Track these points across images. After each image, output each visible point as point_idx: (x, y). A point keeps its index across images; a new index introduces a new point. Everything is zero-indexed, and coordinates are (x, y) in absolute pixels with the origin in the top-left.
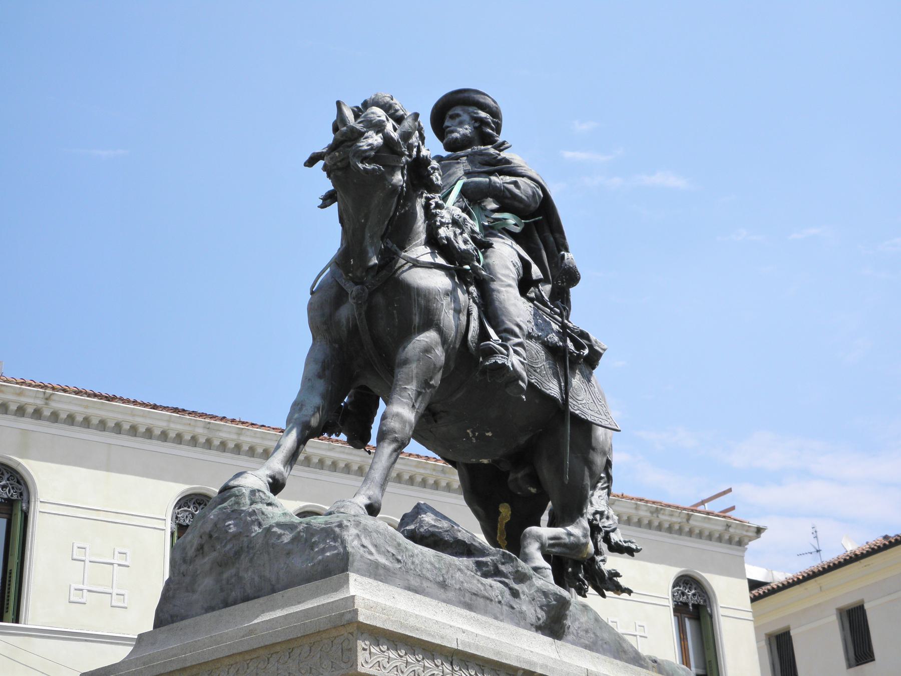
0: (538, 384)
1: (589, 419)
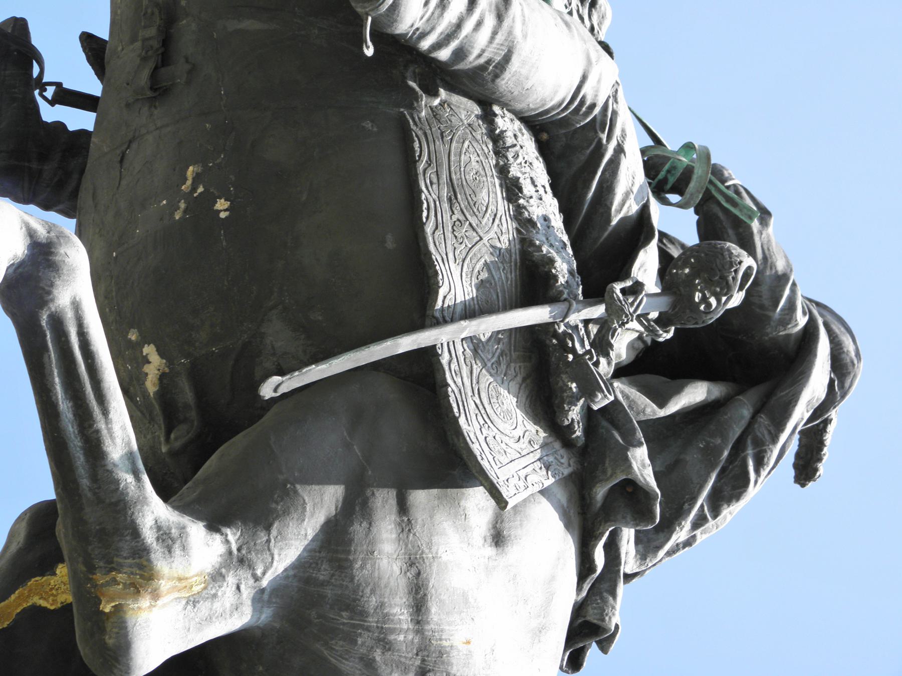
0: (428, 209)
1: (462, 421)
